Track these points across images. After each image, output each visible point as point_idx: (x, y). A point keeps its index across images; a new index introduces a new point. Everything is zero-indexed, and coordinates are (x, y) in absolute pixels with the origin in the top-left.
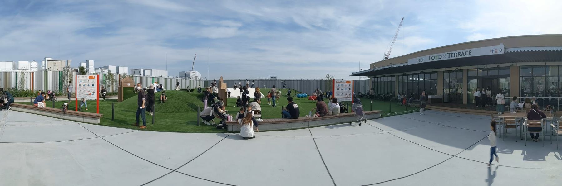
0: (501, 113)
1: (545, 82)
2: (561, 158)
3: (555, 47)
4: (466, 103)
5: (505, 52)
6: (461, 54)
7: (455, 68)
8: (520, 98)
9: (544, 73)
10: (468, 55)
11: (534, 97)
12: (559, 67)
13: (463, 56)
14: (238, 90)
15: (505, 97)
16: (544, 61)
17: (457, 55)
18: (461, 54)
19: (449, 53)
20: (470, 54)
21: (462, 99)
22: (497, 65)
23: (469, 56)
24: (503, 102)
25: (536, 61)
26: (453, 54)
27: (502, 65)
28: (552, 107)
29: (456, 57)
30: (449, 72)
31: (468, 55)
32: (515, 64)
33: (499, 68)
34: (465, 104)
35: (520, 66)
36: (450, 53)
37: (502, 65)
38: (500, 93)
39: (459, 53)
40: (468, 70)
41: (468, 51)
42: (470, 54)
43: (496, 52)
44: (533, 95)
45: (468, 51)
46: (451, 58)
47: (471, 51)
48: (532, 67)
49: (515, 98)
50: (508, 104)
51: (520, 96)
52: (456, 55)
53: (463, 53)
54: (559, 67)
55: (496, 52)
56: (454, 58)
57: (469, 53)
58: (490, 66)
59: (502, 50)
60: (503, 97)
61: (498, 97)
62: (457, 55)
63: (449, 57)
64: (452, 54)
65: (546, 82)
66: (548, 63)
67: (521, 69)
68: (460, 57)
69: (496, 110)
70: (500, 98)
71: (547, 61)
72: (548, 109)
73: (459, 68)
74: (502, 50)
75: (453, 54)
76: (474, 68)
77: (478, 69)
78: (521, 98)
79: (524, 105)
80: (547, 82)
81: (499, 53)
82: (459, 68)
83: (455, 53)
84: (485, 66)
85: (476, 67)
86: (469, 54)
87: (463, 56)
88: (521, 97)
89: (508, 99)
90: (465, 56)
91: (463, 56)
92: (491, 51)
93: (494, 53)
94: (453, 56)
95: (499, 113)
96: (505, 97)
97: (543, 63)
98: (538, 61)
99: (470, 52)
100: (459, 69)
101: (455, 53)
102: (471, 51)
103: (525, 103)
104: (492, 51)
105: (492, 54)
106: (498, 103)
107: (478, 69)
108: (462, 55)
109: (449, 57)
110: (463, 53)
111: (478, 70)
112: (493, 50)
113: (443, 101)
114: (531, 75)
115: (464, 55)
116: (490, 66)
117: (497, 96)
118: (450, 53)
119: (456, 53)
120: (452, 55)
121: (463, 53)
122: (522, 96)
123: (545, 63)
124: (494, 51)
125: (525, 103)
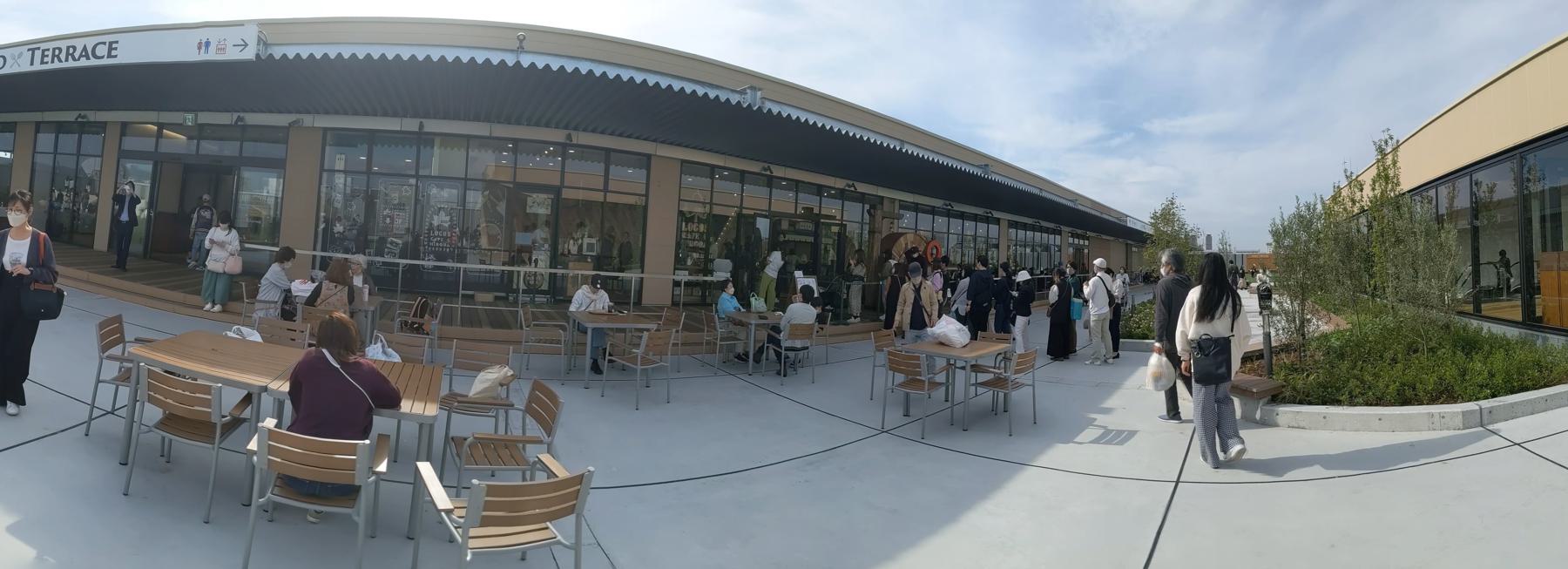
0: (217, 308)
1: (416, 204)
2: (443, 513)
3: (462, 50)
4: (105, 248)
5: (258, 56)
6: (77, 55)
7: (77, 113)
8: (314, 257)
9: (414, 164)
10: (103, 57)
11: (361, 259)
12: (468, 140)
13: (83, 59)
14: (342, 227)
15: (247, 245)
16: (415, 116)
17: (63, 57)
18: (77, 55)
19: (33, 50)
20: (113, 53)
21: (91, 234)
22: (235, 116)
23: (106, 61)
24: (234, 265)
25: (385, 114)
26: (46, 53)
27: (253, 119)
28: (432, 310)
29: (57, 65)
30: (60, 128)
31: (103, 57)
32: (308, 120)
33: (243, 132)
34: (100, 253)
35: (325, 130)
36: (39, 48)
37: (253, 119)
38: (226, 225)
39: (71, 50)
40: (124, 126)
41: (104, 43)
42: (113, 53)
43: (221, 50)
44: (361, 250)
45: (104, 43)
46: (37, 67)
47: (117, 42)
48: (372, 137)
49: (286, 255)
50: (253, 273)
51: (315, 249)
52: (72, 55)
53: (86, 52)
54: (468, 140)
55: (221, 50)
56: (64, 65)
57: (111, 49)
58: (206, 118)
59: (246, 45)
60: (237, 243)
61: (212, 241)
62: (63, 57)
63: (32, 64)
64: (44, 51)
65: (419, 206)
66: (432, 126)
67: (330, 145)
68: (71, 64)
69: (198, 293)
70: (222, 245)
71: (427, 116)
72: (415, 315)
73: (94, 116)
74: (246, 45)
75: (46, 53)
76: (147, 120)
77: (161, 126)
78: (322, 257)
79: (316, 293)
80: (423, 207)
81: (233, 54)
82: (94, 116)
83: (68, 48)
84: (190, 116)
85: (152, 116)
86: (109, 52)
87: (83, 63)
88: (319, 253)
89: (268, 252)
90: (93, 62)
91: (83, 59)
92: (199, 48)
93: (212, 55)
94: (46, 59)
95: (208, 306)
96: (247, 245)
97: (411, 125)
98: (395, 115)
99: (114, 46)
100: (92, 119)
101: (54, 50)
102: (117, 42)
103: (326, 284)
104: (203, 48)
105: (203, 57)
106: (211, 265)
107: (161, 126)
108: (81, 56)
109: (32, 64)
110: (85, 48)
111: (159, 135)
112: (208, 44)
113: (678, 269)
114: (364, 168)
115: (88, 58)
116: (206, 118)
117: (208, 237)
118: (39, 48)
119: (60, 50)
120: (43, 56)
121: (85, 48)
122: (322, 251)
123: (421, 125)
124: (212, 48)
125: (326, 284)
